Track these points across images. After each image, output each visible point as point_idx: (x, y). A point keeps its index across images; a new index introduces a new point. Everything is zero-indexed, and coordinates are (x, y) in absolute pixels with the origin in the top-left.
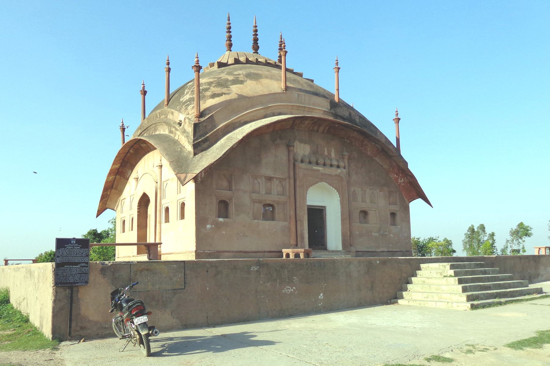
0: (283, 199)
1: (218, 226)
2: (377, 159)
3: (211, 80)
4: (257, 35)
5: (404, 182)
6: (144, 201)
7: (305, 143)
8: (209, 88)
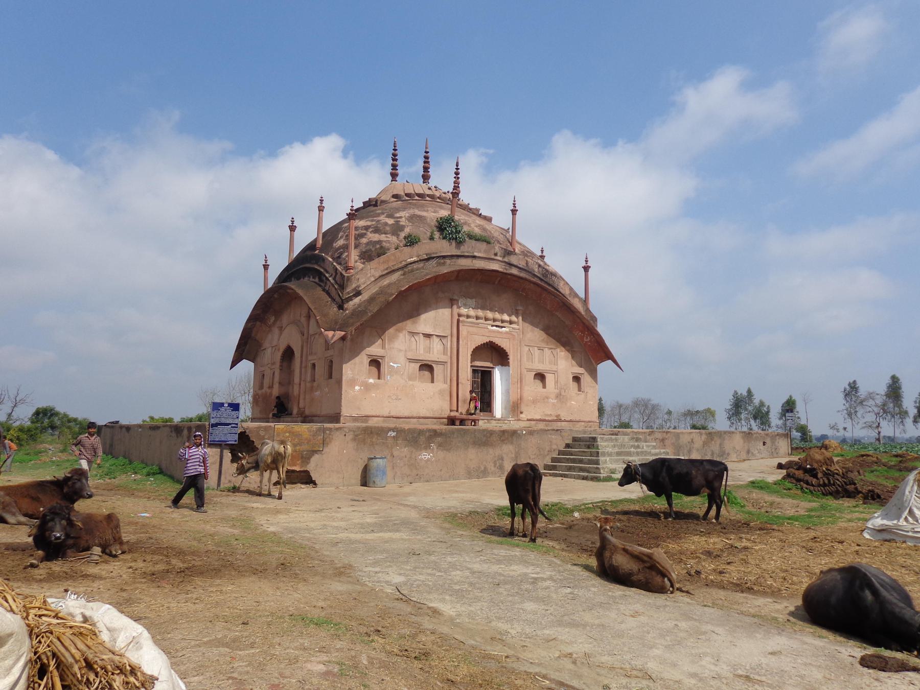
0: (443, 358)
1: (367, 388)
2: (557, 313)
3: (369, 223)
4: (428, 162)
5: (590, 341)
6: (288, 354)
7: (471, 298)
8: (365, 234)
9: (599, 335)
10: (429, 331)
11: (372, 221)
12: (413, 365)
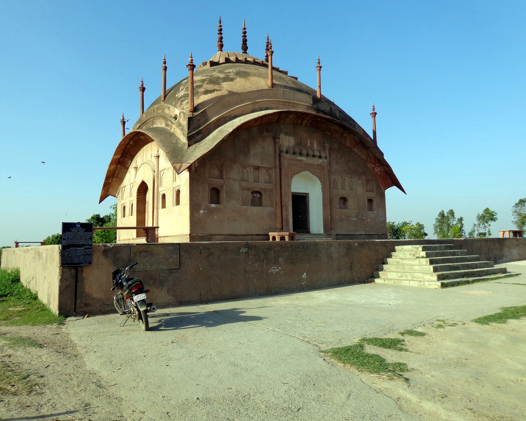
0: (269, 186)
3: (204, 78)
4: (246, 36)
5: (380, 171)
6: (143, 188)
7: (290, 135)
9: (388, 166)
10: (258, 163)
11: (207, 76)
12: (246, 192)
